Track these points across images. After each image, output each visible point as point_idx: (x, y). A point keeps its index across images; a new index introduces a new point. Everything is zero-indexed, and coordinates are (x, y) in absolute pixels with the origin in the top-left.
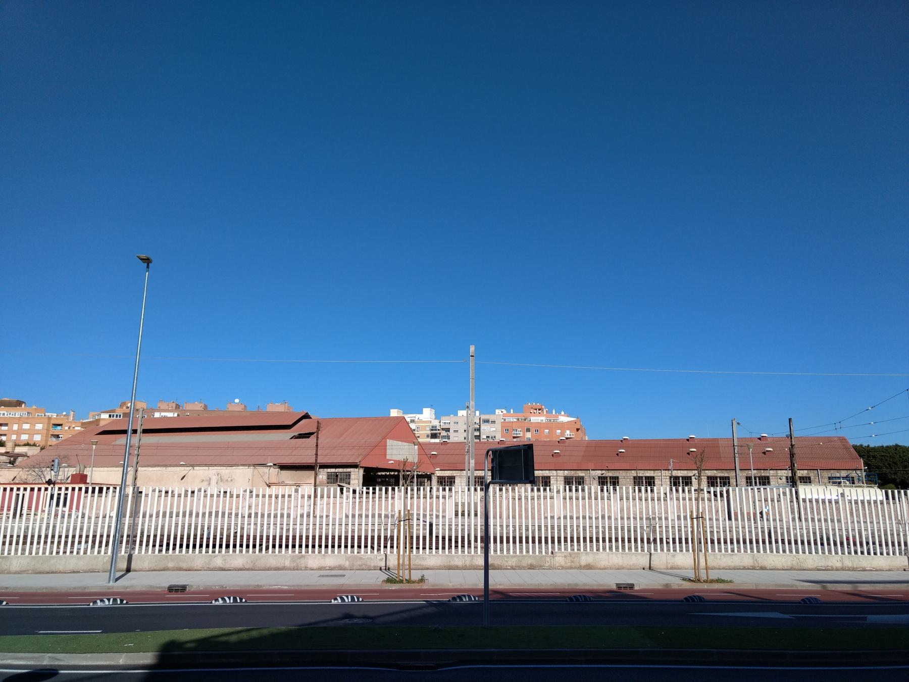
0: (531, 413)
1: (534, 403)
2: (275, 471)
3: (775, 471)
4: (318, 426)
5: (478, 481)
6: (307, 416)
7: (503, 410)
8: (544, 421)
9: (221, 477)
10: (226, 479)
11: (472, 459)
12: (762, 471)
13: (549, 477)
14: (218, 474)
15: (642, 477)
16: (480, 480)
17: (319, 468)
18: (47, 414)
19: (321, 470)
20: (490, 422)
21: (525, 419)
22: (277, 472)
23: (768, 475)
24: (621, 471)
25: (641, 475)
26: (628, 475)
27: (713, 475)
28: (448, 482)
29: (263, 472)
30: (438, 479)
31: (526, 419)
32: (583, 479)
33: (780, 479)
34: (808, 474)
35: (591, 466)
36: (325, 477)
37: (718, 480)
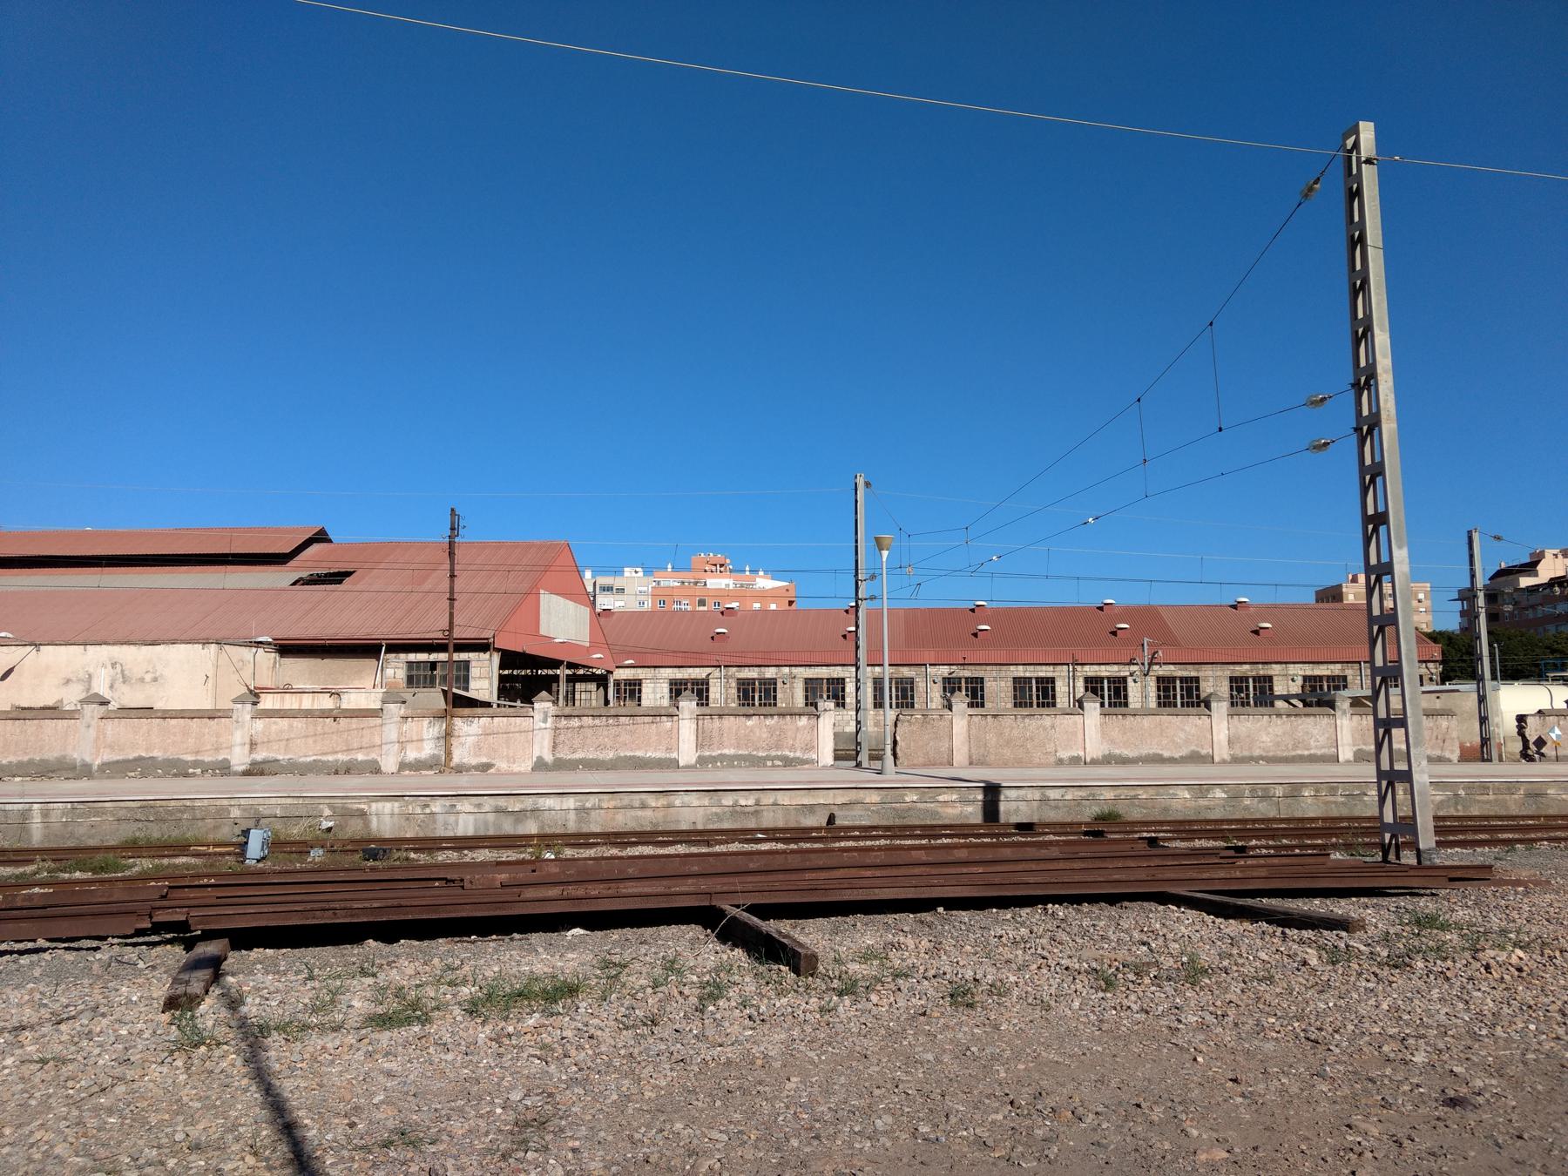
0: (706, 571)
1: (711, 555)
3: (1284, 665)
5: (625, 690)
6: (321, 537)
7: (638, 569)
8: (731, 587)
9: (122, 671)
11: (1400, 547)
12: (1260, 666)
13: (843, 679)
15: (1031, 678)
16: (696, 687)
17: (385, 653)
20: (615, 591)
21: (696, 583)
22: (272, 661)
23: (1270, 673)
24: (989, 668)
25: (1028, 675)
26: (1003, 674)
27: (1167, 674)
28: (625, 693)
30: (671, 684)
31: (697, 582)
32: (912, 683)
33: (1293, 680)
34: (1343, 670)
35: (929, 656)
36: (401, 674)
37: (1178, 682)
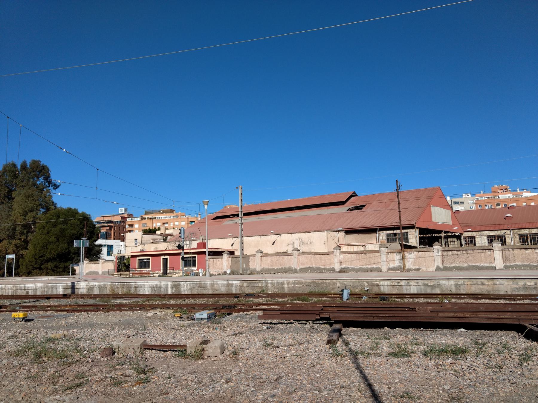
0: (498, 192)
1: (500, 185)
2: (341, 235)
4: (397, 185)
6: (354, 195)
7: (468, 194)
9: (302, 241)
10: (306, 242)
14: (299, 239)
18: (186, 216)
19: (381, 232)
20: (460, 203)
21: (494, 197)
28: (469, 241)
29: (334, 236)
31: (495, 197)
